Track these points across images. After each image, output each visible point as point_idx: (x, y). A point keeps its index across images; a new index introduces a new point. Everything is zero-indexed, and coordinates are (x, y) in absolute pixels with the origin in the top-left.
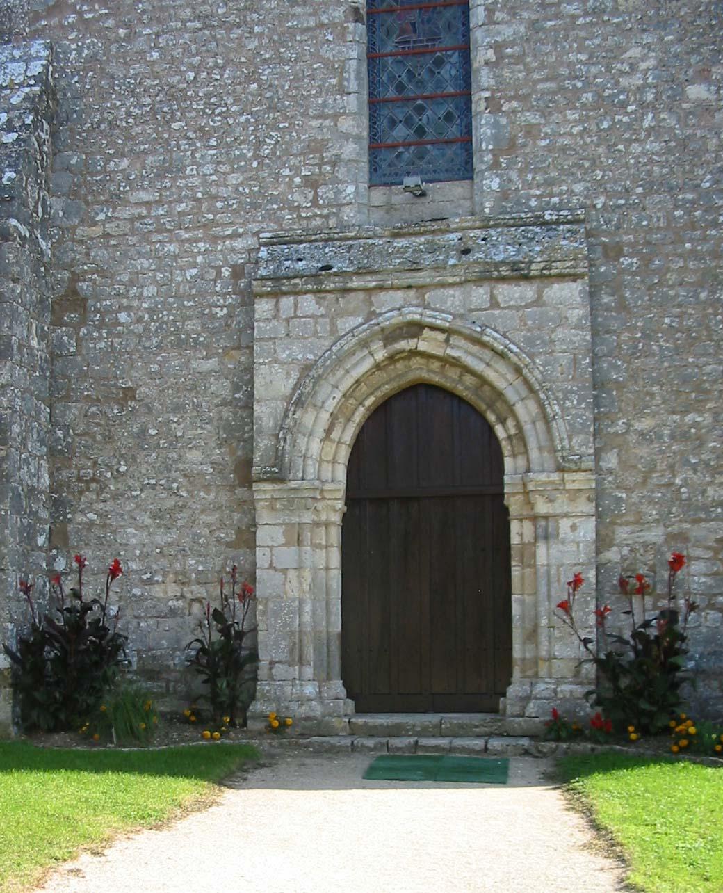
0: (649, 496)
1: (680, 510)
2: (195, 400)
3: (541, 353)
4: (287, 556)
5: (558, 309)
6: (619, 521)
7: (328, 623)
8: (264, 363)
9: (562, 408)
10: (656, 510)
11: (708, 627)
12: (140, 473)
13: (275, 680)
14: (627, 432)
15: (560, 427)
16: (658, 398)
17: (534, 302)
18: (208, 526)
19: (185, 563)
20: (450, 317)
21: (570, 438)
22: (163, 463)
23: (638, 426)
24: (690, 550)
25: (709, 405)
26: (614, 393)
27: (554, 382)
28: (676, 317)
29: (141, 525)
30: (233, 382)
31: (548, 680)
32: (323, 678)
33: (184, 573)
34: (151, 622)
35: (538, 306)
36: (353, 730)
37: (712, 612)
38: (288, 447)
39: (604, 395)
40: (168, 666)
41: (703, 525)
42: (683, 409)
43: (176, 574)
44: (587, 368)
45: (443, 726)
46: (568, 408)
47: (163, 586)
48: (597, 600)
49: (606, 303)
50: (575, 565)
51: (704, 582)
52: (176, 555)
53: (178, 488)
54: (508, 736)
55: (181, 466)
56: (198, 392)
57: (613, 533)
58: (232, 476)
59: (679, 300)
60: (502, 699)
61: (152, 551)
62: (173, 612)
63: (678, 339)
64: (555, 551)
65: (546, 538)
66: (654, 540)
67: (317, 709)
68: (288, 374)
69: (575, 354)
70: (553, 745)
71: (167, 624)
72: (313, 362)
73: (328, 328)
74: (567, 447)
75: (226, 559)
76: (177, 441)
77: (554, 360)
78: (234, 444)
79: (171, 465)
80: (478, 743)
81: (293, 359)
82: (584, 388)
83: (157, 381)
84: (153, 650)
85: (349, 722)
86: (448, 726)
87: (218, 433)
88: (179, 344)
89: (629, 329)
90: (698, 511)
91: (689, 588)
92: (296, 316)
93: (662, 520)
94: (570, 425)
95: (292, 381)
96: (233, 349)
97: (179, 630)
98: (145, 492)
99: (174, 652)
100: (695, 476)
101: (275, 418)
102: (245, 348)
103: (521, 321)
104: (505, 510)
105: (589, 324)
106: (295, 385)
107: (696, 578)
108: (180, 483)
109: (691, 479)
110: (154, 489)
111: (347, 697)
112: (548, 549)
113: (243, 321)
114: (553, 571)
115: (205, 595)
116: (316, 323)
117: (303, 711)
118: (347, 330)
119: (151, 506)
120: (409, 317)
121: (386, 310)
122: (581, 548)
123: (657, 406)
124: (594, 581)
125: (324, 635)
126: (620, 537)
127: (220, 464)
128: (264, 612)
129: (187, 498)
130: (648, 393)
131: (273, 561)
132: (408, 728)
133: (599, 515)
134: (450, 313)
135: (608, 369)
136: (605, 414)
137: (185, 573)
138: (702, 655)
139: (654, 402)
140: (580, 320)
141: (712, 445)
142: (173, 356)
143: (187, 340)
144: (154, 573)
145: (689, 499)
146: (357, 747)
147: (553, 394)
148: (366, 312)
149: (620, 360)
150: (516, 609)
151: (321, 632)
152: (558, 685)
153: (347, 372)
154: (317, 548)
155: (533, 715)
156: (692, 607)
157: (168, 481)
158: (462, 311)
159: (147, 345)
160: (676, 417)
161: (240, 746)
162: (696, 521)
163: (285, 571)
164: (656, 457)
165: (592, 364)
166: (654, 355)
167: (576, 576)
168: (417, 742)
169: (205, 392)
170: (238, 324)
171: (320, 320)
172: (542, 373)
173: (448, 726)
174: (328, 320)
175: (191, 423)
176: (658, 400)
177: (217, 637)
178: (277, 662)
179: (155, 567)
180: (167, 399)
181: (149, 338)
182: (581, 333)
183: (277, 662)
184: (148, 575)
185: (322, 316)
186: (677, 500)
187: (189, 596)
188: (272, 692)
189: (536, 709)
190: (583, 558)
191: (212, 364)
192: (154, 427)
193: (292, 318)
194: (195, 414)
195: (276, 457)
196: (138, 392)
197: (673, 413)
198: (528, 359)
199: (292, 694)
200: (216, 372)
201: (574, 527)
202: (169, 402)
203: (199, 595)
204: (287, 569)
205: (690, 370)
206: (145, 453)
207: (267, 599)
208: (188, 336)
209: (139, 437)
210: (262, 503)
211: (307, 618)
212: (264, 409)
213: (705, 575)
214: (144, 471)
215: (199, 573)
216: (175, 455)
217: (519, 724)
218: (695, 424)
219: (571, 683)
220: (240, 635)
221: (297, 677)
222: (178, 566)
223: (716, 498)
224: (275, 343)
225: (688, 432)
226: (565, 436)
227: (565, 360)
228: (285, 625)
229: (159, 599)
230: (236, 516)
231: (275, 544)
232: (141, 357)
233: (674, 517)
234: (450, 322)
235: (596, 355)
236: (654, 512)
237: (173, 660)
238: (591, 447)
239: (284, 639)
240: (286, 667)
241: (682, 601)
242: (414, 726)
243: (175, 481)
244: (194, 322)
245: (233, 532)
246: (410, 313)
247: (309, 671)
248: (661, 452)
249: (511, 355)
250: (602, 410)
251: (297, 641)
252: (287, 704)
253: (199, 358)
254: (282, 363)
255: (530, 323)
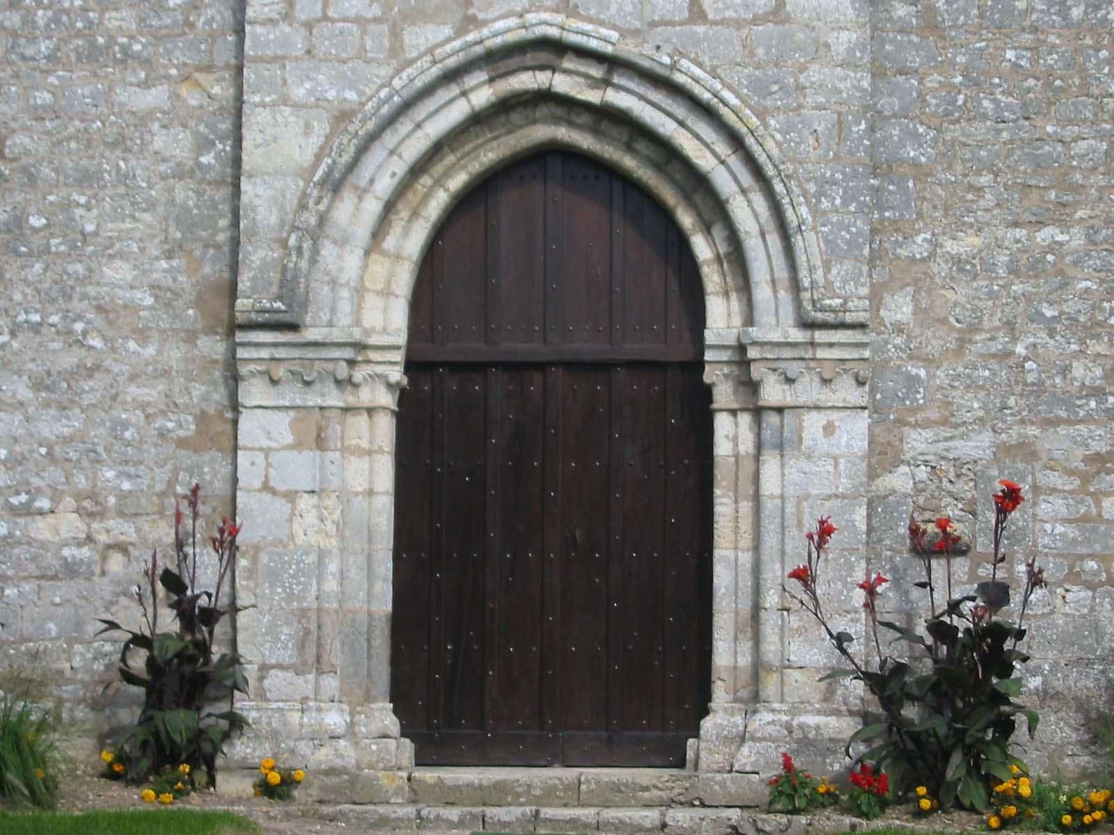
0: (969, 376)
1: (1022, 402)
2: (122, 164)
3: (778, 108)
4: (298, 468)
5: (813, 29)
6: (912, 420)
7: (370, 594)
8: (263, 105)
9: (814, 211)
10: (978, 400)
11: (1067, 615)
12: (11, 299)
13: (267, 700)
14: (932, 255)
15: (809, 246)
16: (988, 196)
17: (767, 14)
18: (143, 406)
19: (95, 474)
20: (614, 35)
21: (827, 267)
22: (56, 282)
23: (950, 246)
24: (1039, 476)
25: (1080, 214)
26: (911, 184)
27: (800, 163)
28: (1027, 49)
29: (10, 401)
30: (196, 134)
31: (777, 706)
32: (358, 700)
33: (93, 496)
34: (27, 587)
35: (776, 23)
36: (416, 793)
37: (1075, 588)
38: (304, 264)
39: (891, 187)
40: (60, 672)
41: (1062, 430)
42: (1033, 219)
43: (78, 496)
44: (861, 138)
45: (583, 787)
46: (824, 213)
47: (50, 519)
48: (868, 561)
49: (900, 18)
50: (829, 498)
51: (1063, 535)
52: (79, 461)
53: (85, 333)
54: (703, 805)
55: (92, 291)
56: (127, 150)
57: (901, 440)
58: (191, 312)
59: (1034, 17)
60: (691, 741)
61: (32, 451)
62: (71, 570)
63: (1029, 91)
64: (793, 470)
65: (780, 447)
66: (975, 454)
67: (346, 753)
68: (308, 128)
69: (840, 114)
70: (784, 819)
71: (61, 591)
72: (356, 107)
73: (386, 43)
74: (821, 281)
75: (175, 471)
76: (84, 241)
77: (802, 122)
78: (198, 253)
79: (72, 288)
80: (651, 817)
81: (318, 99)
82: (855, 175)
83: (48, 124)
84: (30, 641)
85: (409, 779)
86: (593, 786)
87: (166, 231)
88: (93, 55)
89: (939, 67)
90: (1050, 404)
91: (1035, 544)
92: (325, 18)
93: (990, 420)
94: (827, 242)
95: (315, 141)
96: (199, 69)
97: (83, 603)
98: (21, 336)
99: (71, 646)
100: (1052, 342)
101: (282, 209)
102: (222, 69)
103: (744, 47)
104: (707, 393)
105: (867, 59)
106: (322, 148)
107: (1048, 527)
108: (89, 322)
109: (1044, 346)
110: (37, 332)
111: (403, 735)
112: (782, 466)
113: (218, 18)
114: (790, 509)
115: (133, 537)
116: (364, 32)
117: (323, 756)
118: (422, 49)
119: (30, 366)
120: (540, 31)
121: (496, 14)
122: (841, 467)
123: (987, 210)
124: (864, 528)
125: (363, 618)
126: (913, 448)
127: (169, 289)
128: (251, 573)
129: (100, 352)
130: (971, 188)
131: (270, 477)
132: (519, 790)
133: (875, 409)
134: (614, 27)
135: (901, 140)
136: (893, 222)
137: (96, 495)
138: (1055, 666)
139: (982, 202)
140: (851, 51)
141: (1084, 284)
142: (79, 78)
143: (108, 47)
144: (34, 493)
145: (1040, 383)
146: (428, 819)
147: (800, 185)
148: (459, 15)
149: (922, 123)
150: (722, 577)
151: (355, 612)
152: (794, 716)
153: (419, 126)
154: (352, 453)
155: (748, 769)
156: (1036, 579)
157: (65, 318)
158: (638, 24)
159: (29, 52)
160: (1020, 233)
161: (227, 813)
162: (1055, 423)
163: (291, 496)
164: (982, 305)
165: (872, 129)
166: (985, 117)
167: (822, 522)
168: (537, 812)
169: (141, 151)
170: (209, 22)
171: (372, 27)
172: (778, 144)
173: (593, 786)
174: (385, 28)
175: (114, 209)
176: (989, 199)
177: (169, 622)
178: (273, 667)
179: (36, 481)
180: (67, 160)
181: (33, 40)
182: (852, 74)
183: (273, 667)
184: (23, 498)
185: (376, 20)
186: (1017, 383)
187: (103, 538)
188: (265, 721)
189: (753, 759)
190: (844, 485)
191: (156, 97)
192: (40, 213)
193: (318, 21)
194: (122, 190)
195: (283, 283)
196: (8, 143)
197: (1016, 224)
198: (754, 119)
199: (301, 725)
200: (163, 113)
201: (829, 429)
202: (70, 165)
203: (122, 538)
204: (296, 492)
205: (1047, 148)
206: (20, 261)
207: (257, 548)
208: (111, 39)
209: (10, 231)
210: (252, 367)
211: (331, 585)
212: (260, 190)
213: (1065, 521)
214: (18, 297)
215: (123, 496)
216: (80, 268)
217: (723, 784)
218: (1054, 247)
219: (819, 712)
220: (210, 616)
221: (312, 696)
222: (82, 482)
223: (1087, 383)
224: (284, 67)
225: (1043, 260)
226: (819, 263)
227: (822, 123)
228: (290, 597)
229: (43, 545)
230: (198, 390)
231: (274, 445)
232: (16, 76)
233: (1012, 415)
234: (613, 44)
235: (879, 113)
236: (976, 405)
237: (69, 660)
238: (863, 285)
239: (288, 623)
240: (290, 675)
241: (1022, 568)
242: (529, 786)
243: (79, 318)
244: (124, 13)
245: (190, 419)
246: (541, 23)
247: (331, 684)
248: (991, 295)
249: (724, 111)
250: (887, 214)
251: (313, 627)
252: (291, 744)
253: (131, 84)
254: (297, 106)
255: (760, 51)
